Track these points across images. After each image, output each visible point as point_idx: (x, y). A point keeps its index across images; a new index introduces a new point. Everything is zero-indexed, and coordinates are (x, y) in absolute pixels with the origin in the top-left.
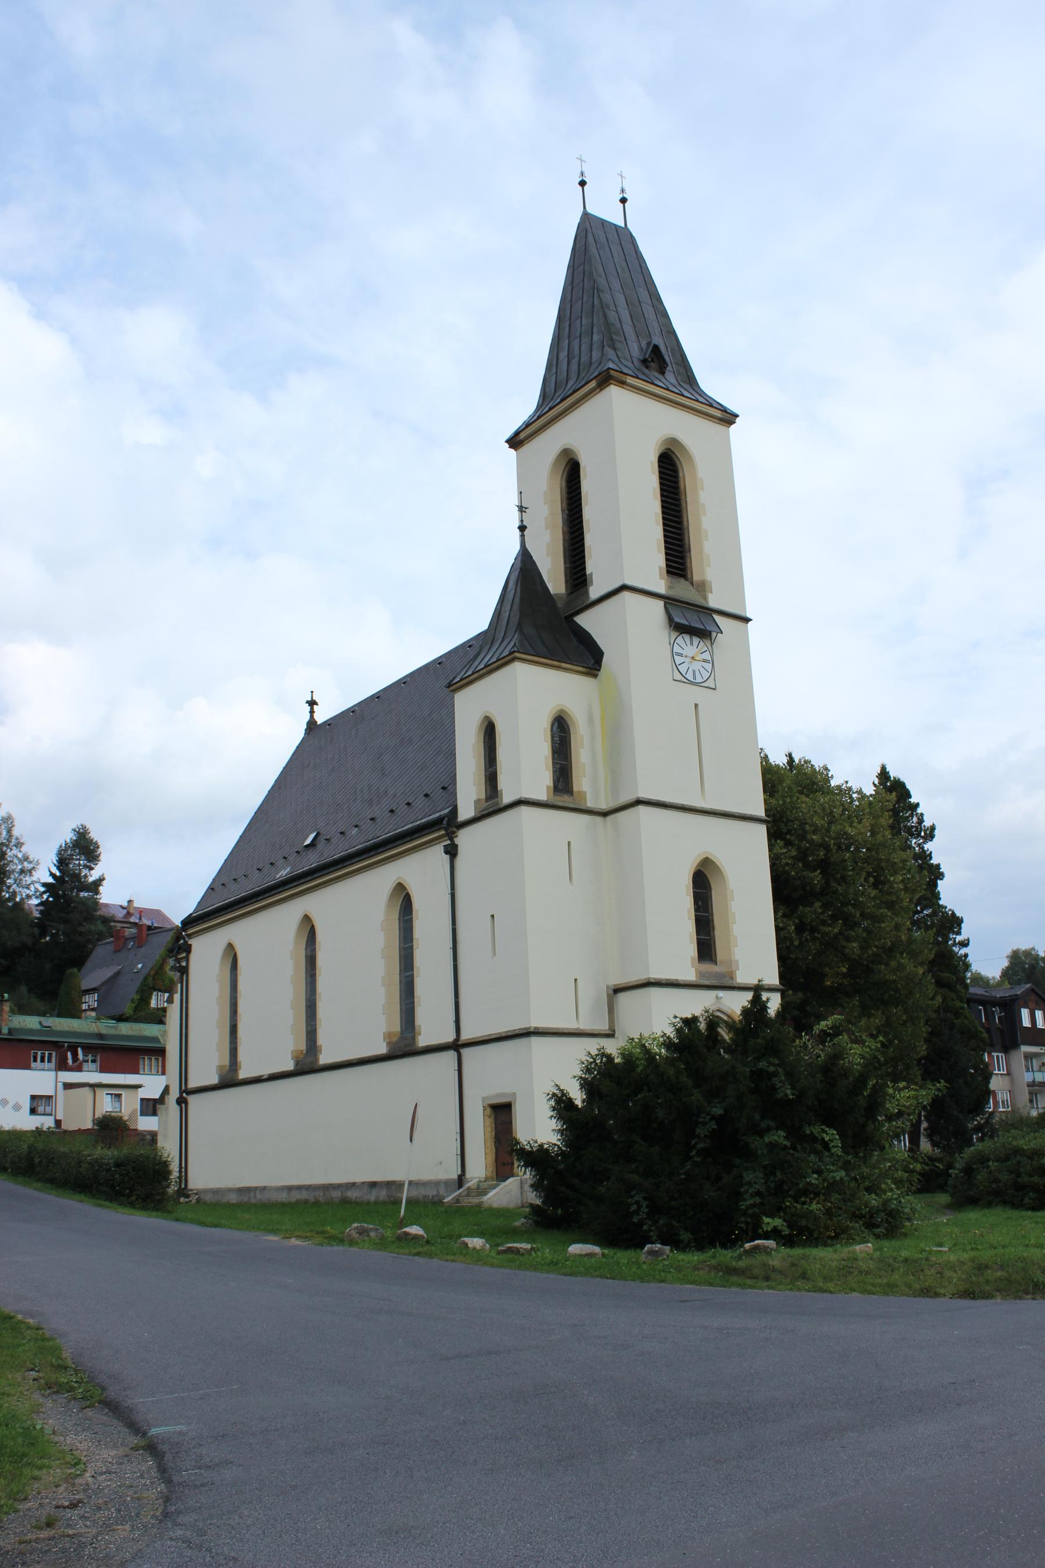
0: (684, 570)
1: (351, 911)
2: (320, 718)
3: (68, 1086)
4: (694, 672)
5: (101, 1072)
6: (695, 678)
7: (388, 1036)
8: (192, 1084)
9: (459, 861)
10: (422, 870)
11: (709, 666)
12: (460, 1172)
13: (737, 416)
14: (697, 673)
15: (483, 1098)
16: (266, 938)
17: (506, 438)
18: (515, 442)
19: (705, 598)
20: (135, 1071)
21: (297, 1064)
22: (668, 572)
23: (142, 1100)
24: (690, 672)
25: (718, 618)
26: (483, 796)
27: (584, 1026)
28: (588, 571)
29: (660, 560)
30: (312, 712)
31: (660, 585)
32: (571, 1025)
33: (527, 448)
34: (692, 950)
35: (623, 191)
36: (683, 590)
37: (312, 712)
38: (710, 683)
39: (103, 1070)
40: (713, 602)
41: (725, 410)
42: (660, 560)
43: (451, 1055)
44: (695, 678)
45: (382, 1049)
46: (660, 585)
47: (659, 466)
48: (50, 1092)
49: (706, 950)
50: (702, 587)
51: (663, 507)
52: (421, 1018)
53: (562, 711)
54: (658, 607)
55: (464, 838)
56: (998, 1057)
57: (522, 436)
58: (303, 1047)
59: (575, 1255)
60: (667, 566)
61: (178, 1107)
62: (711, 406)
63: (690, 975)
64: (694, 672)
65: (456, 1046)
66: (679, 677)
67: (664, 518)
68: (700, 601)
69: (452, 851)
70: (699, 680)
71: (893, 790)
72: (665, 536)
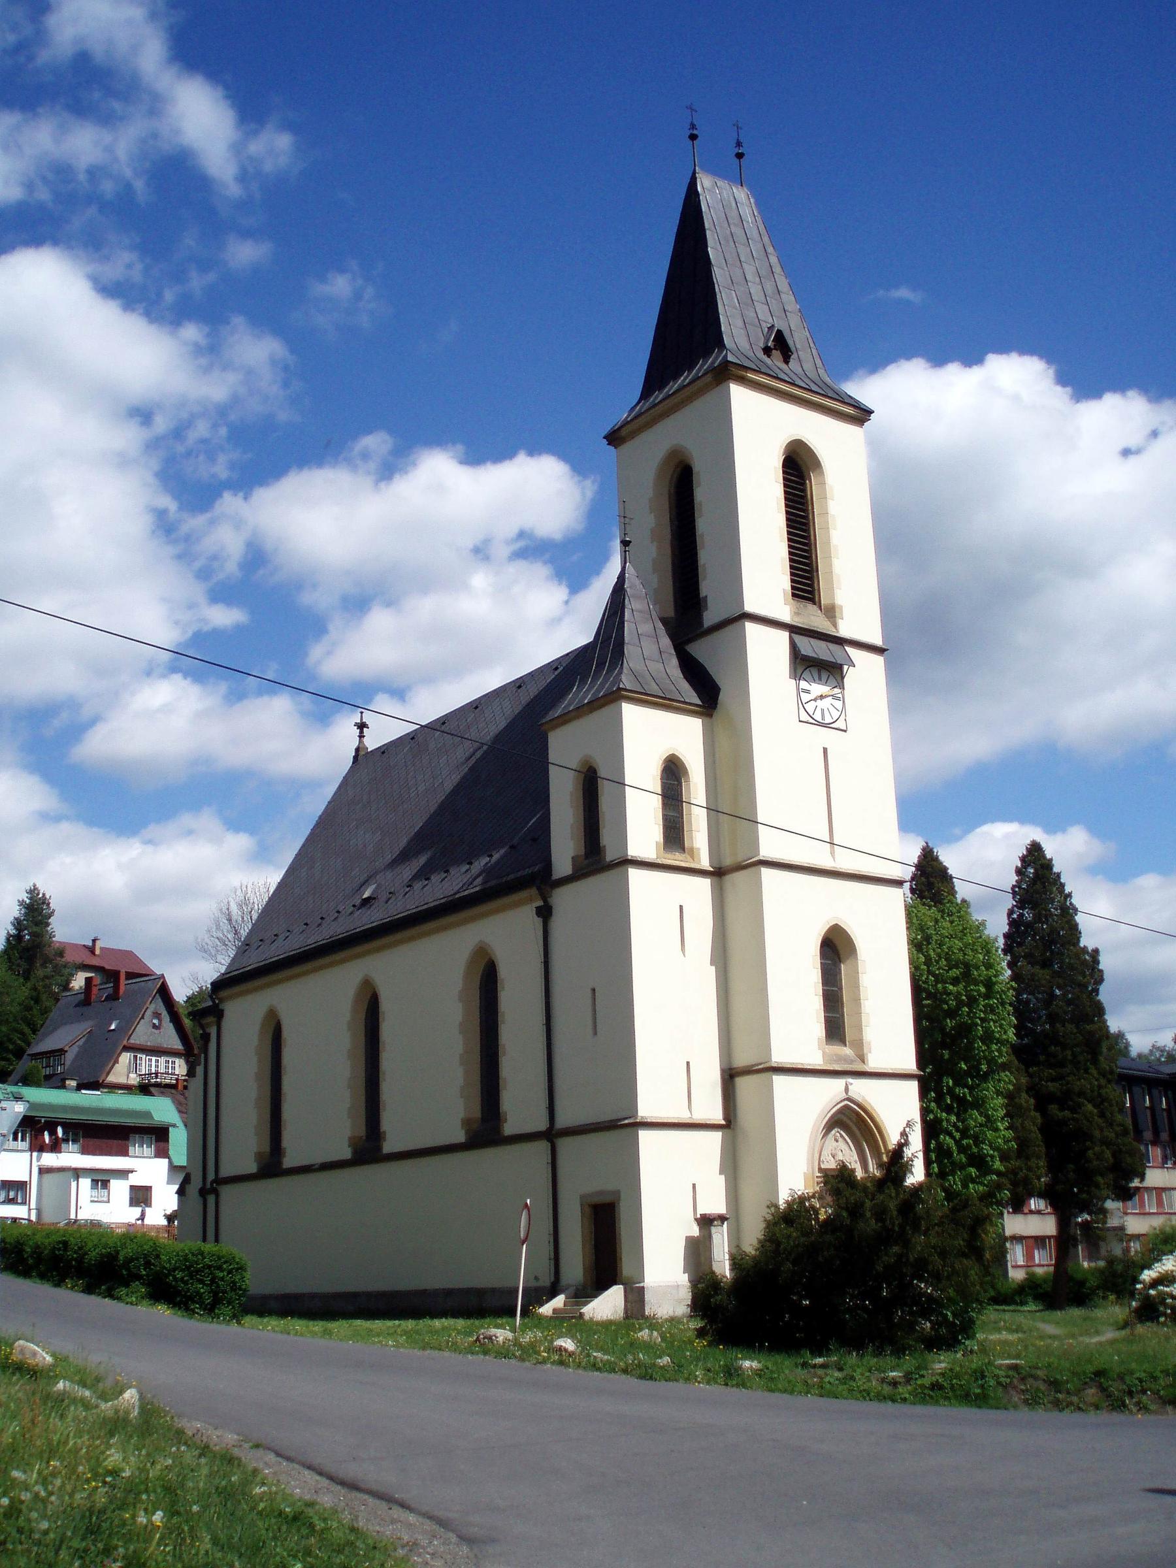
0: (812, 592)
1: (424, 982)
2: (372, 742)
3: (43, 1171)
4: (823, 710)
5: (83, 1153)
6: (823, 718)
7: (467, 1123)
8: (227, 1170)
9: (556, 923)
10: (508, 931)
11: (839, 704)
12: (553, 1279)
13: (870, 412)
14: (826, 712)
15: (582, 1197)
16: (318, 1008)
17: (605, 433)
18: (615, 438)
19: (835, 625)
20: (124, 1153)
21: (355, 1152)
22: (794, 595)
23: (132, 1187)
24: (818, 712)
25: (850, 650)
26: (582, 852)
27: (699, 1116)
28: (703, 593)
29: (785, 582)
30: (361, 736)
31: (784, 611)
32: (683, 1116)
33: (627, 447)
34: (819, 1029)
35: (739, 144)
36: (814, 619)
37: (361, 736)
38: (840, 724)
39: (85, 1151)
40: (845, 630)
41: (857, 405)
42: (784, 581)
43: (543, 1146)
44: (823, 718)
45: (460, 1137)
46: (784, 611)
47: (784, 472)
48: (24, 1177)
49: (835, 1029)
50: (831, 613)
51: (788, 519)
52: (508, 1101)
53: (673, 755)
54: (782, 638)
55: (564, 900)
56: (798, 467)
57: (624, 432)
58: (362, 1131)
59: (15, 1479)
60: (793, 588)
61: (200, 1200)
62: (843, 402)
63: (815, 1059)
64: (823, 710)
65: (551, 1135)
66: (804, 717)
67: (789, 533)
68: (831, 631)
69: (545, 913)
70: (828, 720)
71: (1096, 951)
72: (790, 553)
